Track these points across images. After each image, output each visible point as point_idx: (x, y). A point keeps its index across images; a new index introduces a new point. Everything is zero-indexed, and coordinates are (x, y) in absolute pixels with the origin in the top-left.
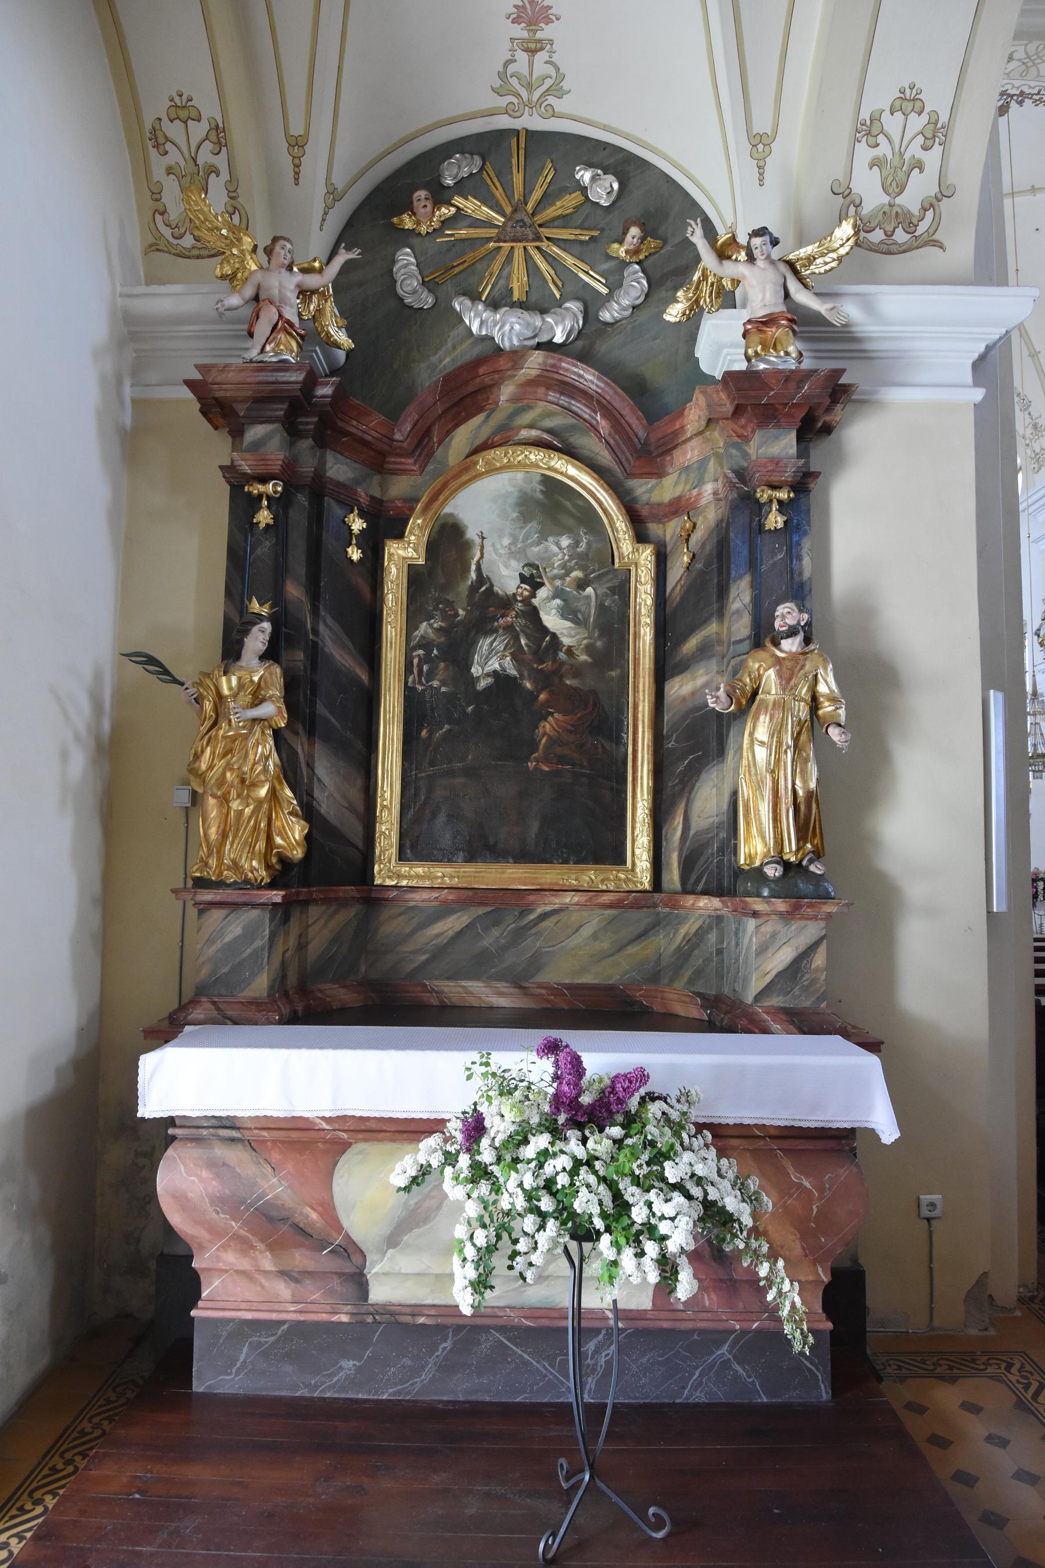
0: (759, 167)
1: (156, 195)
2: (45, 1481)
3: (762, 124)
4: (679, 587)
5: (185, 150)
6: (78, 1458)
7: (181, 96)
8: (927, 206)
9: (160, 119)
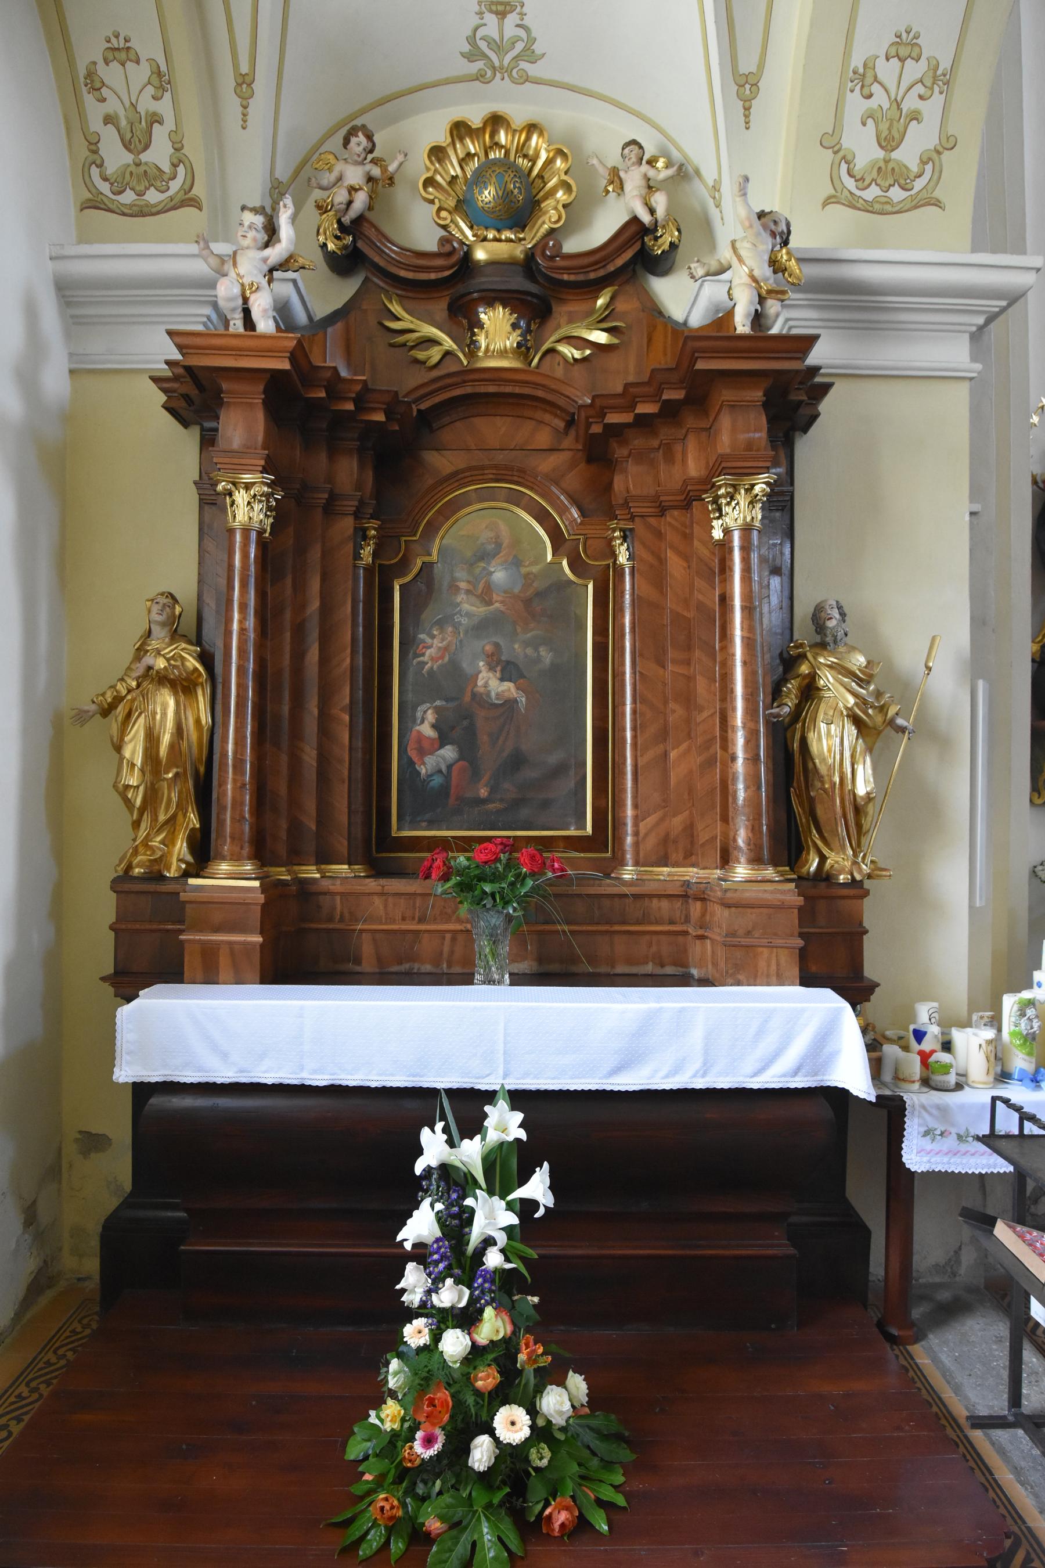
0: (745, 109)
1: (93, 147)
2: (12, 1407)
3: (747, 65)
6: (42, 1387)
7: (117, 37)
8: (175, 161)
9: (95, 63)
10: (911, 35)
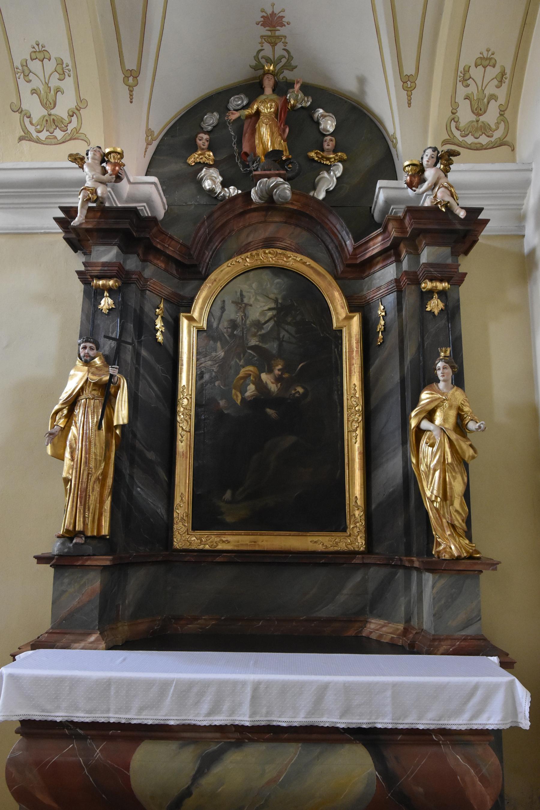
3: (409, 69)
4: (414, 461)
5: (42, 78)
7: (38, 45)
10: (490, 53)
